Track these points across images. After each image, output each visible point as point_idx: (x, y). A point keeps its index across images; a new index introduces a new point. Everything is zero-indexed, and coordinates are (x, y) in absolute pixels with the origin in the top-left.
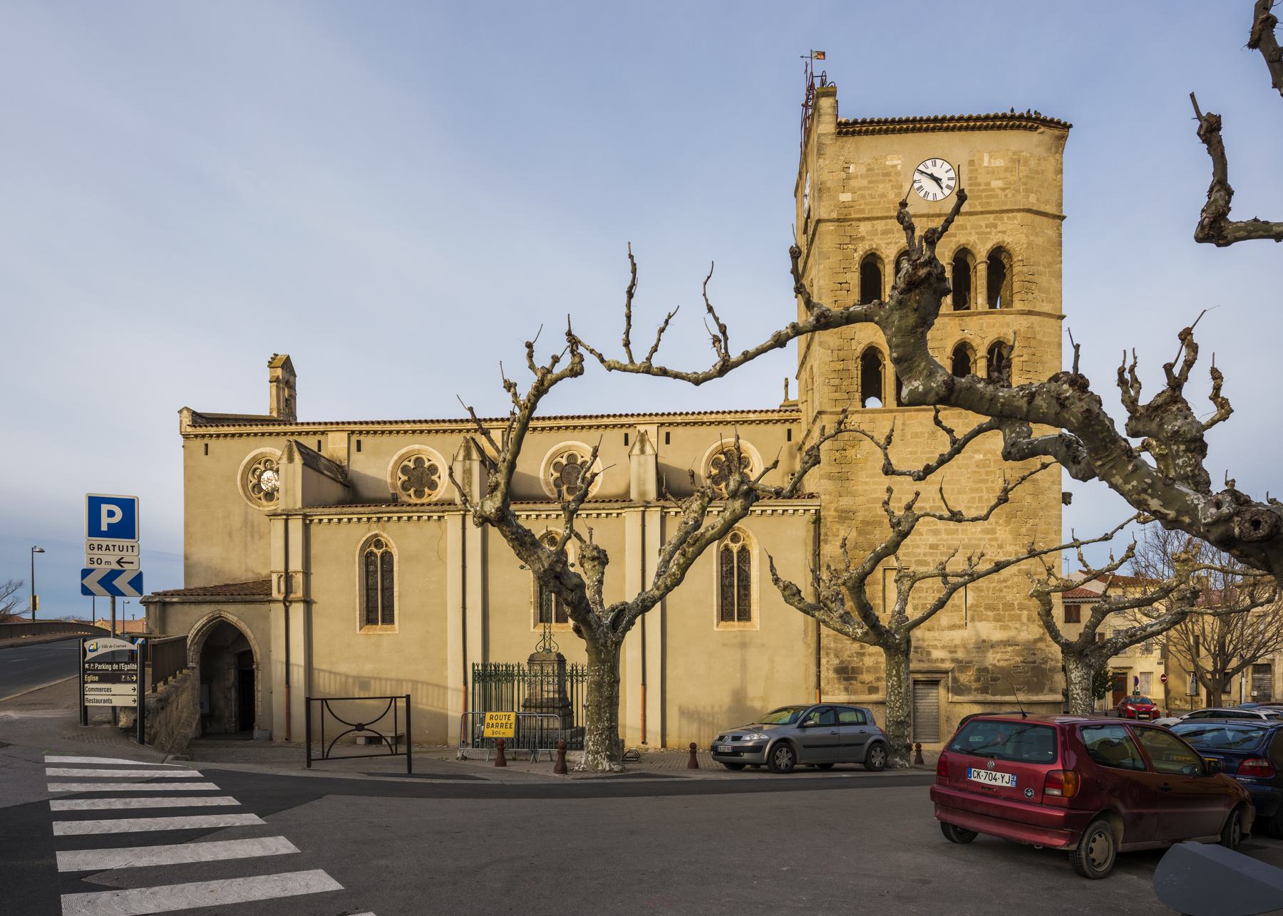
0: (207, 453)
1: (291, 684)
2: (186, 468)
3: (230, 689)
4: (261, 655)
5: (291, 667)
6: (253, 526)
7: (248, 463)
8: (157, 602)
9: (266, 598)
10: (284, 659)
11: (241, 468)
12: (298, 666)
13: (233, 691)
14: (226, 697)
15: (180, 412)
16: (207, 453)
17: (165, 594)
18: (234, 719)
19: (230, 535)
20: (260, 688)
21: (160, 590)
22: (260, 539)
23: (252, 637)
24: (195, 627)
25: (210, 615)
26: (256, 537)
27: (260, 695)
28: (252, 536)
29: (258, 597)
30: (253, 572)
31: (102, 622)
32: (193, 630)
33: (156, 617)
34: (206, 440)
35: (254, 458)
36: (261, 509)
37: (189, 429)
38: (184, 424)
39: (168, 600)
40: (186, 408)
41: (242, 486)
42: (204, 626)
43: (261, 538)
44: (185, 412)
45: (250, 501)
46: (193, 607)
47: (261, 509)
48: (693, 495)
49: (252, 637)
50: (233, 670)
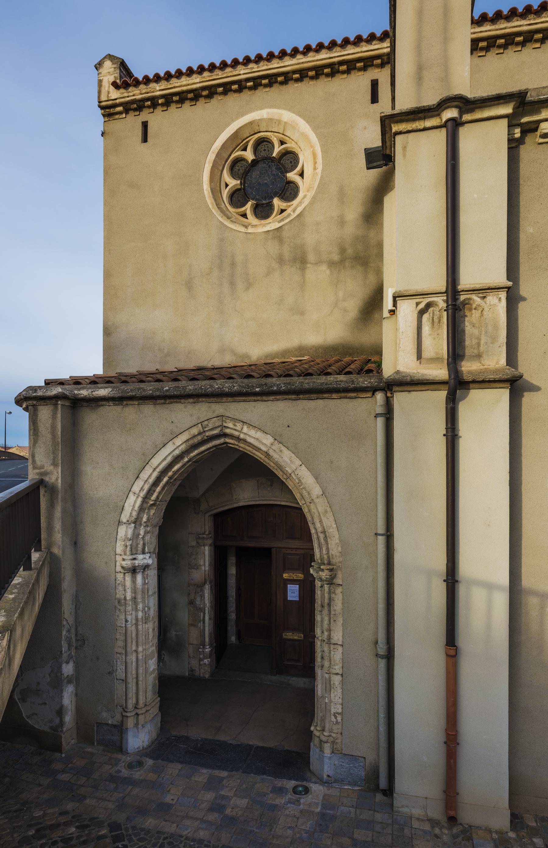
0: (145, 139)
1: (462, 641)
2: (107, 172)
3: (200, 586)
4: (343, 542)
5: (462, 590)
6: (233, 264)
7: (224, 146)
8: (56, 397)
9: (364, 381)
10: (504, 579)
11: (211, 156)
12: (490, 587)
13: (207, 587)
14: (191, 603)
15: (99, 66)
16: (145, 139)
17: (77, 382)
18: (208, 650)
19: (189, 285)
20: (337, 636)
21: (65, 375)
22: (247, 289)
23: (316, 490)
24: (155, 462)
25: (195, 431)
26: (240, 285)
27: (337, 655)
28: (232, 284)
29: (323, 379)
30: (233, 352)
31: (17, 447)
32: (147, 471)
33: (54, 436)
34: (145, 115)
35: (235, 135)
36: (250, 230)
37: (115, 94)
38: (106, 84)
39: (84, 393)
40: (110, 57)
41: (213, 191)
42: (177, 459)
43: (249, 286)
44: (108, 64)
45: (228, 218)
46: (148, 409)
47: (250, 230)
48: (312, 376)
49: (316, 490)
50: (207, 548)
